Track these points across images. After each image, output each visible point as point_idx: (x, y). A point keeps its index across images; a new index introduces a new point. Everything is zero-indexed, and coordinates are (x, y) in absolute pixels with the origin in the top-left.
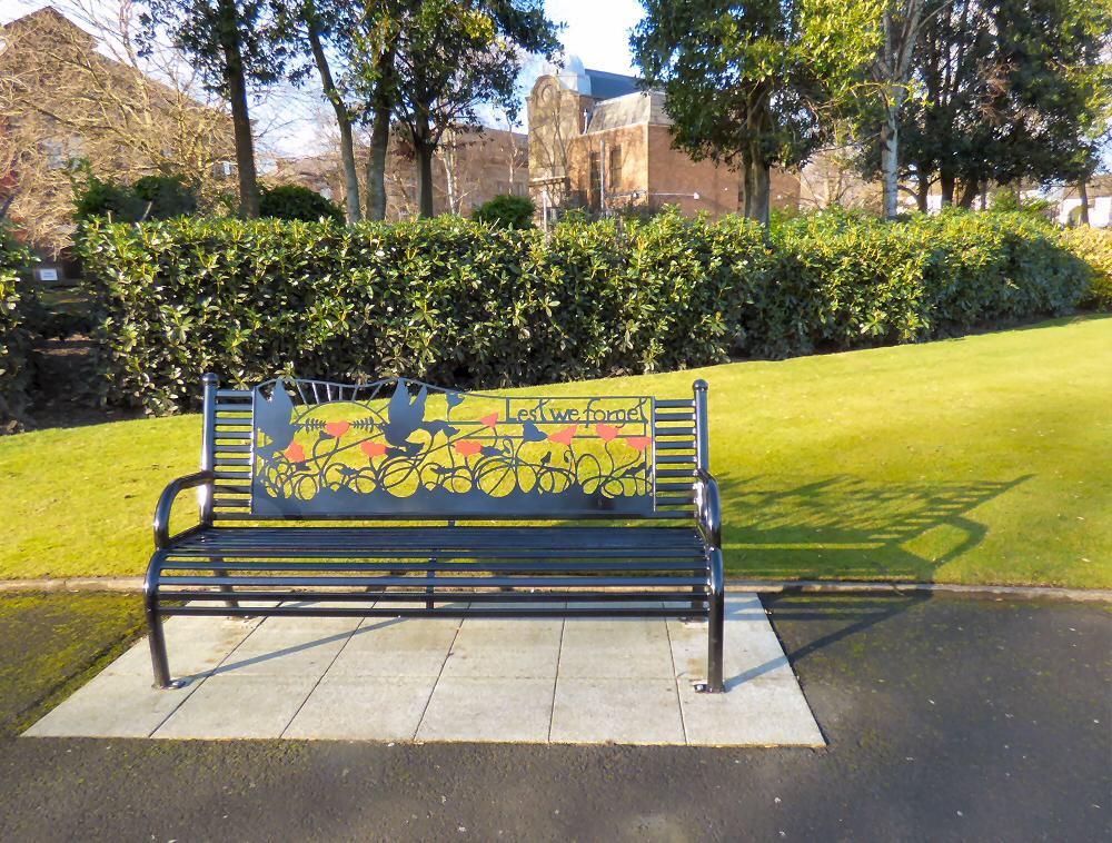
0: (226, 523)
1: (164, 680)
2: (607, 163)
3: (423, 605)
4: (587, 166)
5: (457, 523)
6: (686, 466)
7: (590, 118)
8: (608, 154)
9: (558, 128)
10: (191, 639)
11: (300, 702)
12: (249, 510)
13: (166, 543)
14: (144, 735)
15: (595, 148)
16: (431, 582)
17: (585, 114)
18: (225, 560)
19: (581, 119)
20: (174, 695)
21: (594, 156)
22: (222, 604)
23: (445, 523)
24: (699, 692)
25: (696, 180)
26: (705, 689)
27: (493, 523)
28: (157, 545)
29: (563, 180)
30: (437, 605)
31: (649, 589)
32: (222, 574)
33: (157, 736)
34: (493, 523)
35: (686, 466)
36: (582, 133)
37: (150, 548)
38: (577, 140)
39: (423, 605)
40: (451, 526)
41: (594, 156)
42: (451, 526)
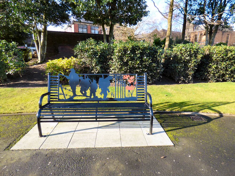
0: (52, 102)
1: (41, 135)
2: (199, 37)
3: (95, 120)
4: (195, 37)
5: (99, 102)
6: (143, 91)
7: (195, 28)
8: (199, 35)
9: (188, 30)
10: (47, 127)
11: (95, 140)
12: (57, 100)
13: (42, 107)
14: (37, 148)
15: (196, 34)
16: (96, 115)
17: (194, 28)
18: (53, 111)
19: (194, 28)
20: (43, 139)
21: (196, 35)
22: (52, 120)
23: (97, 102)
24: (148, 135)
25: (218, 40)
26: (149, 134)
27: (86, 102)
28: (39, 108)
29: (189, 40)
30: (98, 119)
31: (138, 116)
32: (52, 114)
33: (41, 148)
34: (86, 102)
35: (143, 91)
36: (193, 31)
37: (38, 109)
38: (193, 32)
39: (95, 120)
40: (98, 103)
41: (196, 35)
42: (98, 103)
